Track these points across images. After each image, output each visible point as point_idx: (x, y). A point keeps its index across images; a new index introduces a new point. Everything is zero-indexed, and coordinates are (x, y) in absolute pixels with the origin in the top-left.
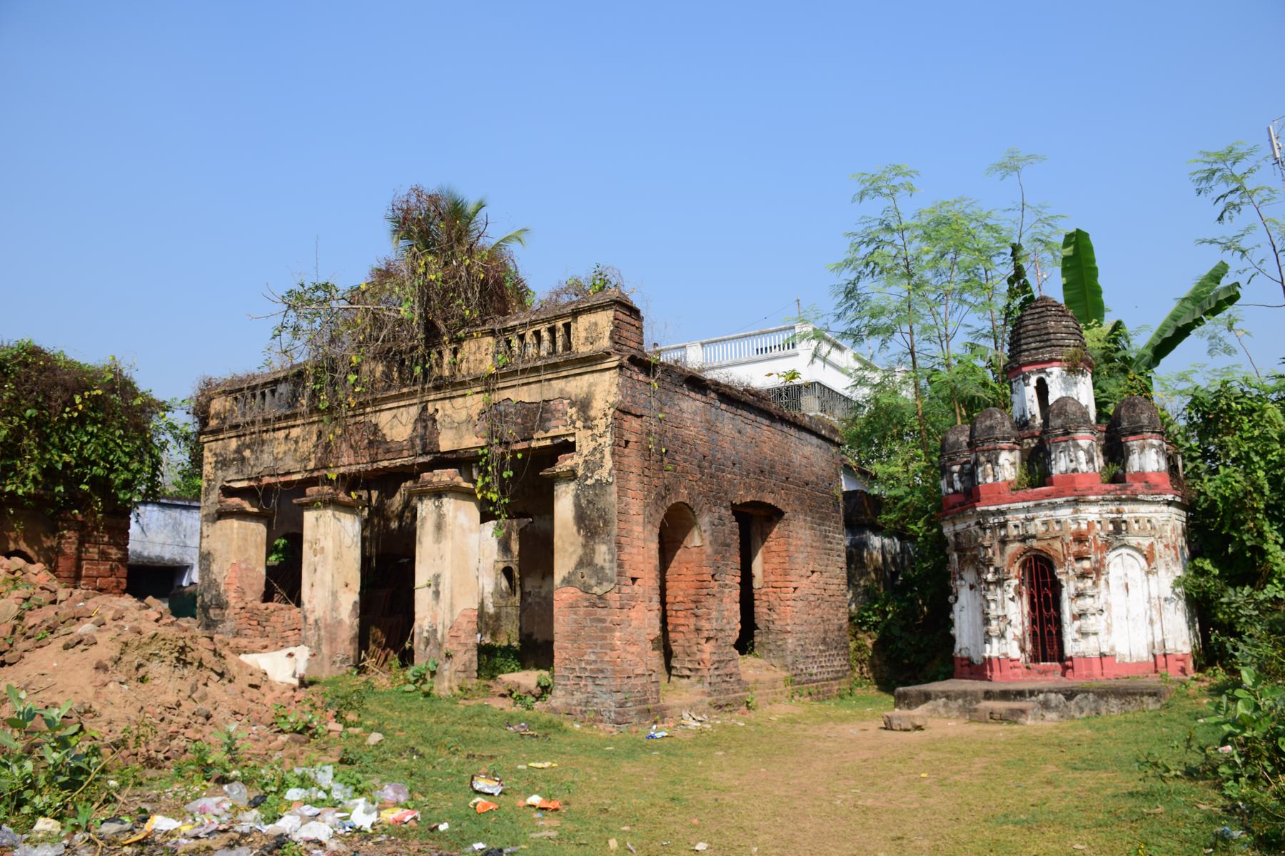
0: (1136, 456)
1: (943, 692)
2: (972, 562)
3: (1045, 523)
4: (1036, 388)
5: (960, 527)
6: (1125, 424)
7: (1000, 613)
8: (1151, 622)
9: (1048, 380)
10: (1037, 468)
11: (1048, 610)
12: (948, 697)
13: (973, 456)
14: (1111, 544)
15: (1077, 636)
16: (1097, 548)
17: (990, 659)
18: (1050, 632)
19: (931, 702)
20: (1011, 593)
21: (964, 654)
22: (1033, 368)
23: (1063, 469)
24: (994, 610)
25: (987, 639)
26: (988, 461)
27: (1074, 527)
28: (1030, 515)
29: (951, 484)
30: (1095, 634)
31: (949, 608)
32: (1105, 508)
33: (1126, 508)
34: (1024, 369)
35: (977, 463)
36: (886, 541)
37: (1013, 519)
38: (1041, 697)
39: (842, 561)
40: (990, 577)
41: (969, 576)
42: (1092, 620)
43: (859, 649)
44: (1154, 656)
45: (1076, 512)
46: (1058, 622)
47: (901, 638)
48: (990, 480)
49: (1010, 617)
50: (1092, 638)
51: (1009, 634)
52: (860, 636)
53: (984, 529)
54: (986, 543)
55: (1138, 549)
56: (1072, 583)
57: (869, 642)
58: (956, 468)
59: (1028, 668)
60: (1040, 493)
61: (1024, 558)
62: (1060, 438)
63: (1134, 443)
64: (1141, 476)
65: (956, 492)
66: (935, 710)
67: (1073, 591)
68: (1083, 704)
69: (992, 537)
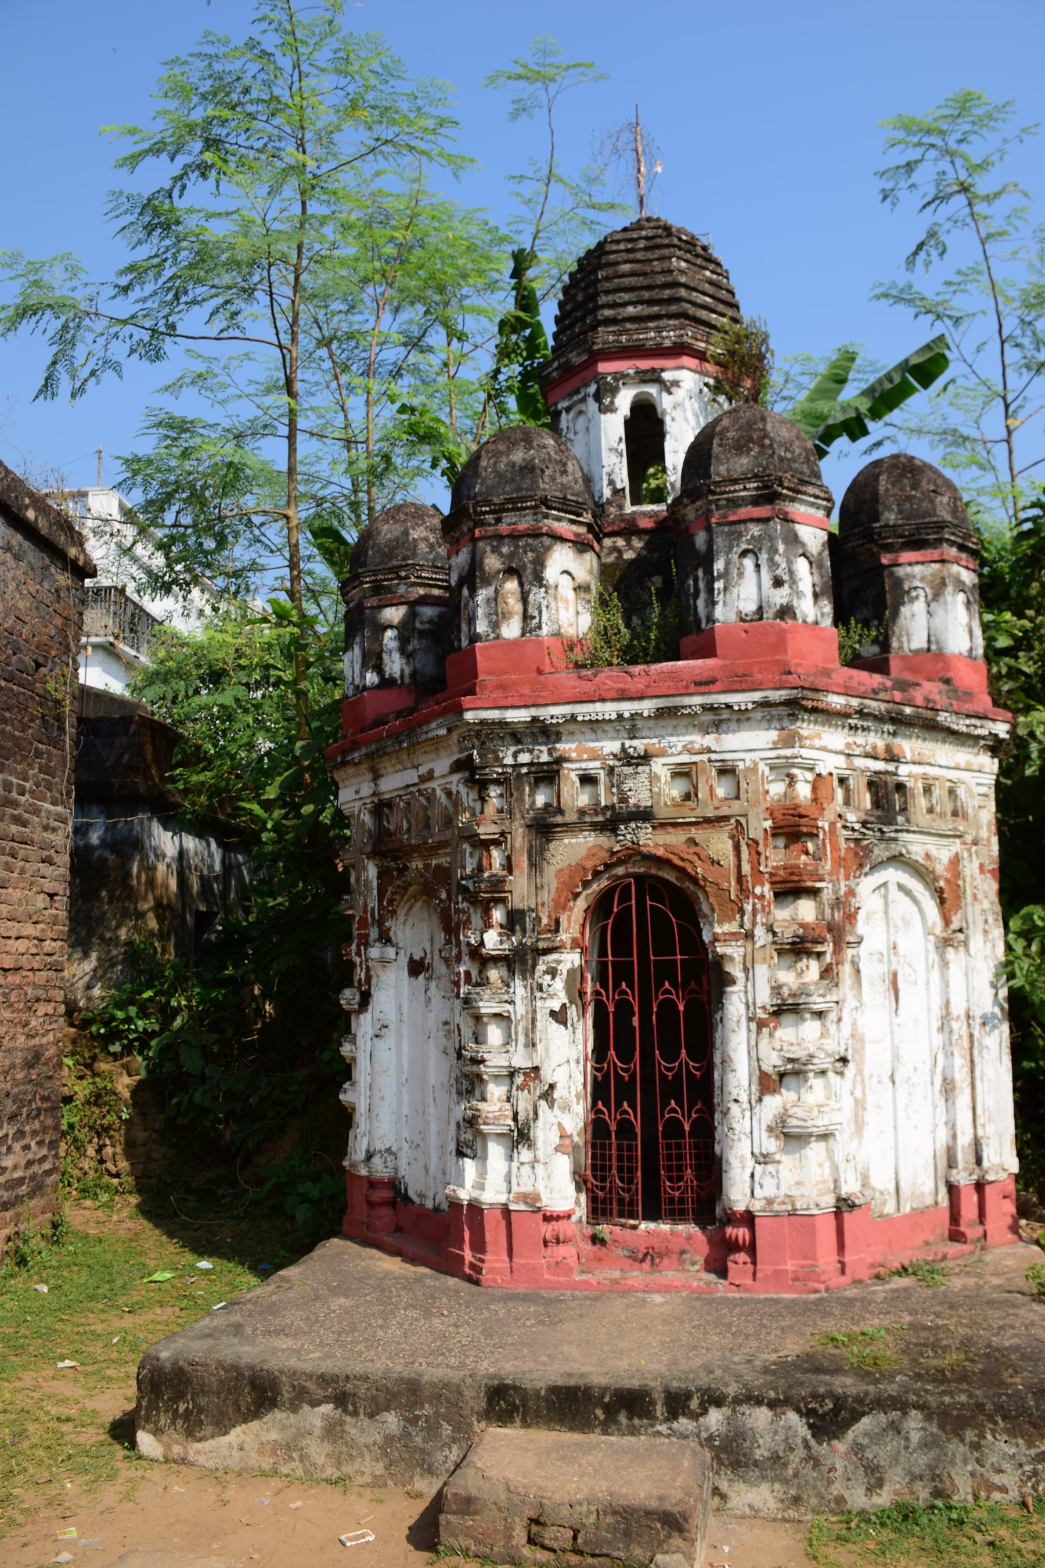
0: (919, 607)
1: (324, 1380)
2: (428, 892)
3: (682, 772)
4: (629, 424)
5: (394, 781)
6: (891, 517)
7: (520, 1059)
8: (948, 1089)
9: (665, 402)
10: (659, 597)
11: (671, 1055)
12: (341, 1400)
13: (462, 558)
14: (868, 850)
15: (771, 1145)
16: (839, 862)
17: (475, 1208)
18: (674, 1126)
19: (278, 1415)
20: (558, 994)
21: (380, 1168)
22: (627, 366)
23: (749, 607)
24: (496, 1049)
25: (469, 1140)
26: (511, 571)
27: (777, 789)
28: (639, 745)
29: (373, 659)
30: (825, 1137)
31: (341, 1024)
32: (860, 739)
33: (909, 746)
34: (603, 367)
35: (473, 577)
36: (191, 843)
37: (585, 754)
38: (715, 1418)
39: (57, 876)
40: (492, 940)
41: (414, 932)
42: (815, 1091)
43: (97, 1099)
44: (952, 1189)
45: (790, 740)
46: (703, 1093)
47: (203, 1078)
48: (511, 630)
49: (548, 1075)
50: (815, 1151)
51: (545, 1134)
52: (103, 1066)
53: (481, 786)
54: (486, 830)
55: (922, 872)
56: (762, 972)
57: (124, 1084)
58: (394, 614)
59: (595, 1239)
60: (672, 675)
61: (604, 883)
62: (745, 512)
63: (915, 569)
64: (933, 659)
65: (387, 683)
66: (290, 1448)
67: (764, 997)
68: (881, 1453)
69: (507, 812)
